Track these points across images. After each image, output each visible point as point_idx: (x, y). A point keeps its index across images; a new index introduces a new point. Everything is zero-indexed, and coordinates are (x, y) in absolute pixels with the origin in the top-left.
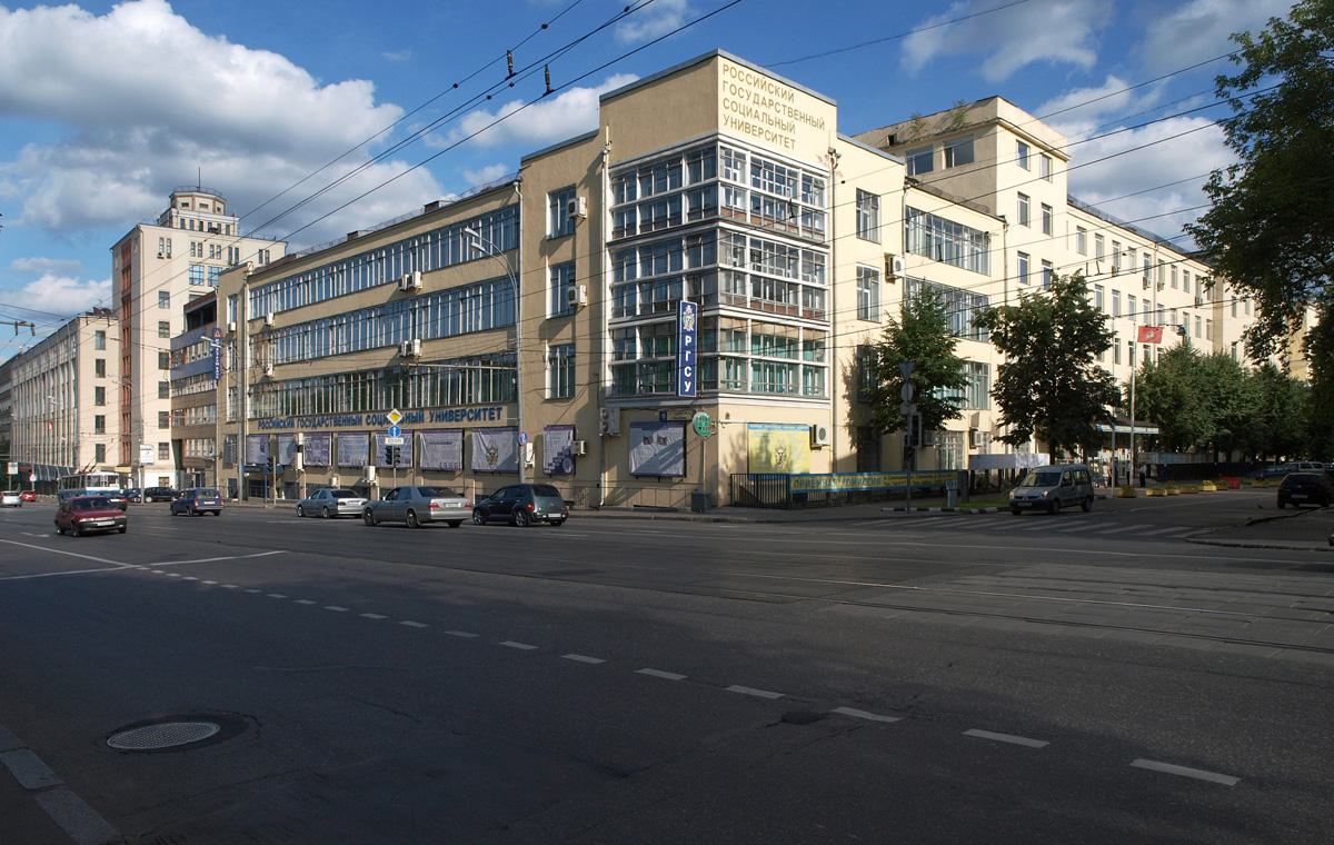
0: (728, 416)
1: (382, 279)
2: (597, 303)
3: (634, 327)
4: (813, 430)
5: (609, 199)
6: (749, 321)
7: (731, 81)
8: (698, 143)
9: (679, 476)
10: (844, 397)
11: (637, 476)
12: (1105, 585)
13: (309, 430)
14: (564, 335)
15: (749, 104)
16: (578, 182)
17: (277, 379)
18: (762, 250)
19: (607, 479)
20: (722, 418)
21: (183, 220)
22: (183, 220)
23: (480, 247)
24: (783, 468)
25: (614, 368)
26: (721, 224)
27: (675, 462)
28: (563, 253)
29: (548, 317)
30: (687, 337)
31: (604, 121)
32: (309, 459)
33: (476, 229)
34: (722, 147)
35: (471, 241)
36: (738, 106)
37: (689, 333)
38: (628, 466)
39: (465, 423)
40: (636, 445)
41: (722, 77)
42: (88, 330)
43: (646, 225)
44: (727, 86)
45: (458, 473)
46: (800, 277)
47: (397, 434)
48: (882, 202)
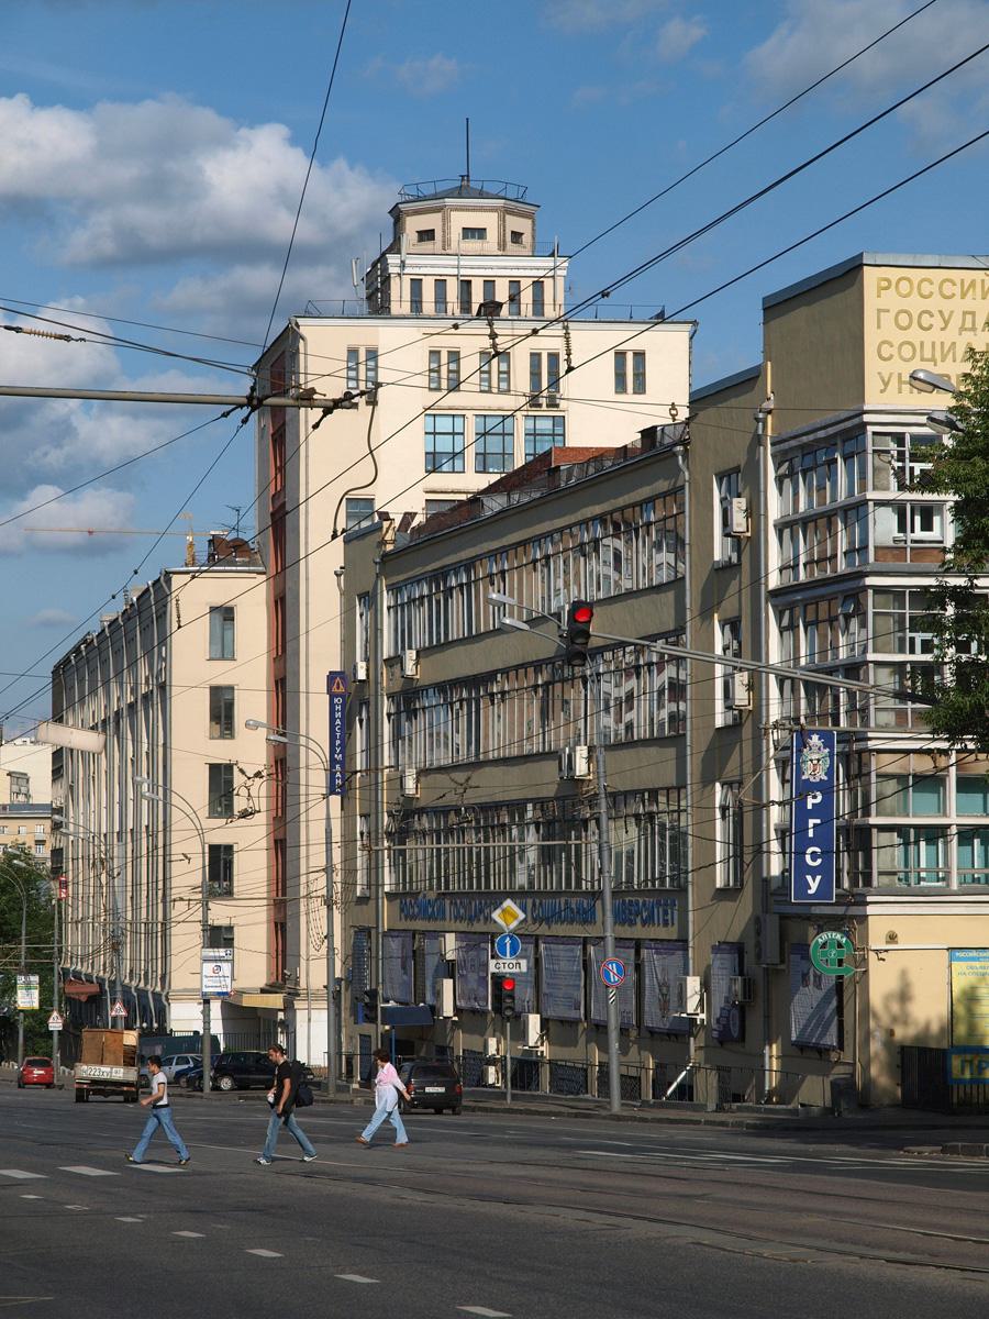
0: (892, 938)
12: (628, 1168)
13: (463, 926)
17: (422, 804)
19: (773, 1055)
20: (876, 939)
21: (416, 284)
22: (416, 284)
26: (869, 581)
32: (462, 996)
34: (874, 433)
42: (194, 597)
47: (514, 951)
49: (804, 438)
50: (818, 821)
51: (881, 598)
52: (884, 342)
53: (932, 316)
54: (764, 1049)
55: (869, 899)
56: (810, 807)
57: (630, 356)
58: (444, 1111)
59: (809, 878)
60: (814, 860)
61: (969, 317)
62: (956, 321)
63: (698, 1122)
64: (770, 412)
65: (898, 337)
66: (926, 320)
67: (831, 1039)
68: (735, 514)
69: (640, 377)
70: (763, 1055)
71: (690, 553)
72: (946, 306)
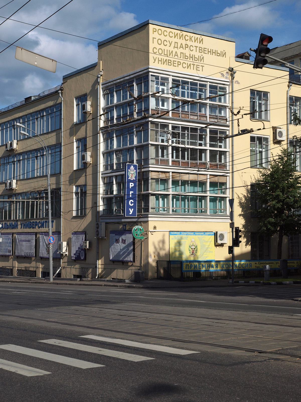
0: (155, 228)
1: (43, 130)
2: (95, 165)
3: (112, 176)
4: (216, 234)
5: (102, 103)
6: (171, 173)
7: (158, 37)
8: (140, 73)
9: (131, 262)
10: (240, 215)
11: (113, 261)
12: (130, 312)
14: (81, 181)
15: (171, 49)
16: (88, 92)
18: (180, 132)
19: (100, 263)
20: (151, 229)
23: (26, 133)
24: (180, 259)
25: (103, 199)
26: (150, 119)
27: (129, 254)
28: (81, 133)
29: (75, 168)
30: (131, 183)
31: (100, 58)
33: (23, 123)
34: (152, 75)
35: (20, 130)
36: (163, 51)
37: (132, 181)
38: (109, 257)
39: (36, 230)
40: (113, 244)
41: (152, 35)
43: (118, 118)
44: (155, 41)
45: (33, 259)
46: (208, 145)
48: (271, 97)
49: (115, 82)
50: (133, 192)
51: (152, 125)
52: (154, 48)
53: (167, 42)
54: (97, 262)
55: (149, 216)
56: (130, 188)
59: (130, 209)
60: (131, 204)
61: (176, 44)
62: (173, 45)
63: (101, 285)
64: (101, 75)
65: (158, 47)
66: (165, 43)
67: (130, 258)
68: (88, 106)
70: (96, 264)
71: (63, 121)
72: (171, 40)
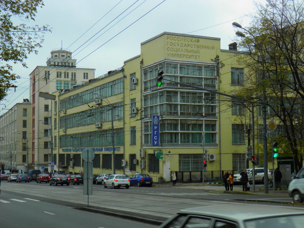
57: (86, 74)
58: (80, 184)
59: (155, 142)
60: (156, 138)
69: (87, 76)
